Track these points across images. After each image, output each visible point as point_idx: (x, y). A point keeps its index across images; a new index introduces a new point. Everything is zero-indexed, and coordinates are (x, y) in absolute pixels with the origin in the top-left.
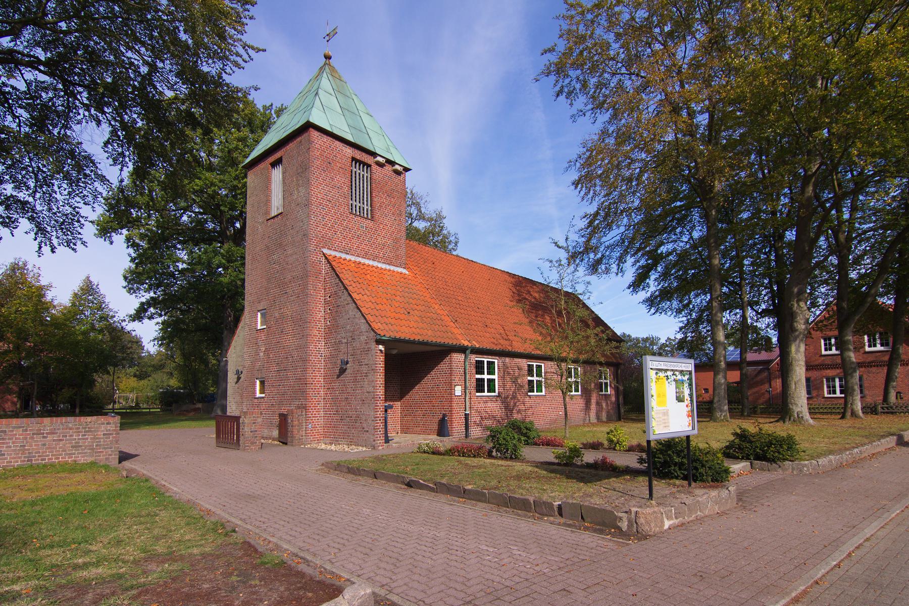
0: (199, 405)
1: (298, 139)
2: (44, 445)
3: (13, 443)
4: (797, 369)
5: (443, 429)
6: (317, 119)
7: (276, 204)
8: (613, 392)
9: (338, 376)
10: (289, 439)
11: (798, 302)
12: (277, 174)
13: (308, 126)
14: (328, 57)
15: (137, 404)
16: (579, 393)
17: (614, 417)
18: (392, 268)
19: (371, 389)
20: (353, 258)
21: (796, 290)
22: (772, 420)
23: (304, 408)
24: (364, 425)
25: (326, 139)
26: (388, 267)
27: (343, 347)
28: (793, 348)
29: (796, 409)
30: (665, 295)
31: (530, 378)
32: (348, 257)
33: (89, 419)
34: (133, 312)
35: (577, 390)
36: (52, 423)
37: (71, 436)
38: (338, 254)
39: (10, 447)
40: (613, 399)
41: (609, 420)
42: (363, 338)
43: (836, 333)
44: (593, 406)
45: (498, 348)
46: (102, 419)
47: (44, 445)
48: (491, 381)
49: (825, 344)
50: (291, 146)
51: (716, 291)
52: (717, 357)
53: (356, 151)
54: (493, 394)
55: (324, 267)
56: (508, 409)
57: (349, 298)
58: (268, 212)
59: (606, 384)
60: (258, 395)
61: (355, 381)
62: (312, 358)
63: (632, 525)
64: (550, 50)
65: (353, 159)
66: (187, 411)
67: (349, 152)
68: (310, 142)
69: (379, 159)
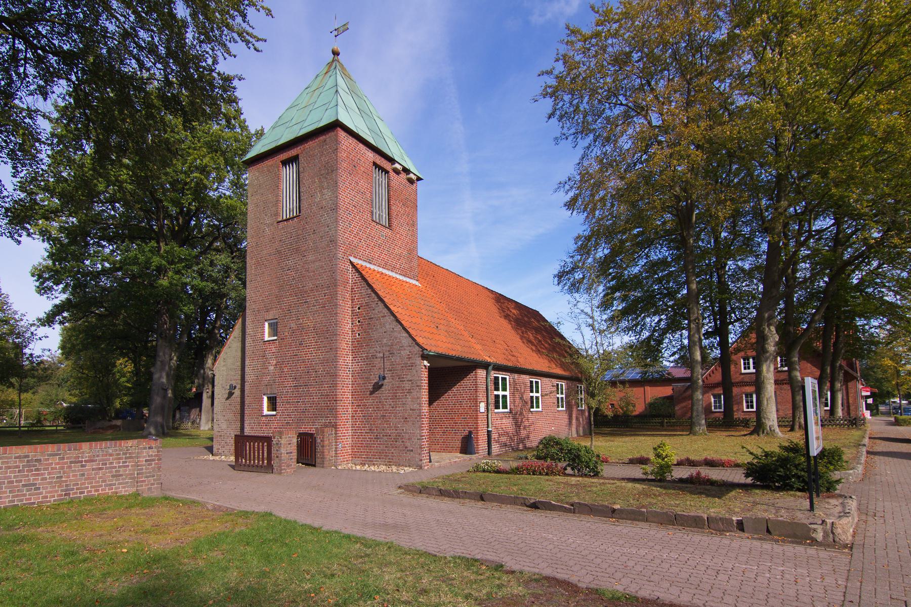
0: (119, 422)
1: (322, 138)
2: (83, 475)
3: (49, 474)
4: (769, 386)
5: (467, 446)
7: (288, 205)
9: (372, 393)
10: (318, 461)
11: (768, 326)
12: (288, 174)
13: (336, 125)
14: (336, 53)
15: (39, 421)
19: (416, 406)
20: (376, 268)
21: (766, 315)
22: (743, 433)
23: (335, 426)
24: (408, 444)
25: (351, 140)
28: (765, 368)
29: (768, 423)
31: (496, 393)
33: (130, 443)
34: (42, 315)
37: (111, 463)
38: (364, 264)
39: (46, 479)
40: (587, 414)
41: (585, 435)
42: (405, 353)
43: (754, 353)
44: (574, 421)
46: (144, 443)
47: (83, 475)
48: (504, 397)
49: (744, 364)
50: (311, 144)
51: (694, 313)
52: (695, 375)
53: (377, 156)
55: (351, 274)
58: (277, 214)
60: (266, 412)
61: (395, 397)
62: (341, 373)
63: (828, 535)
64: (549, 73)
65: (375, 164)
66: (103, 429)
67: (371, 156)
68: (337, 142)
69: (397, 165)
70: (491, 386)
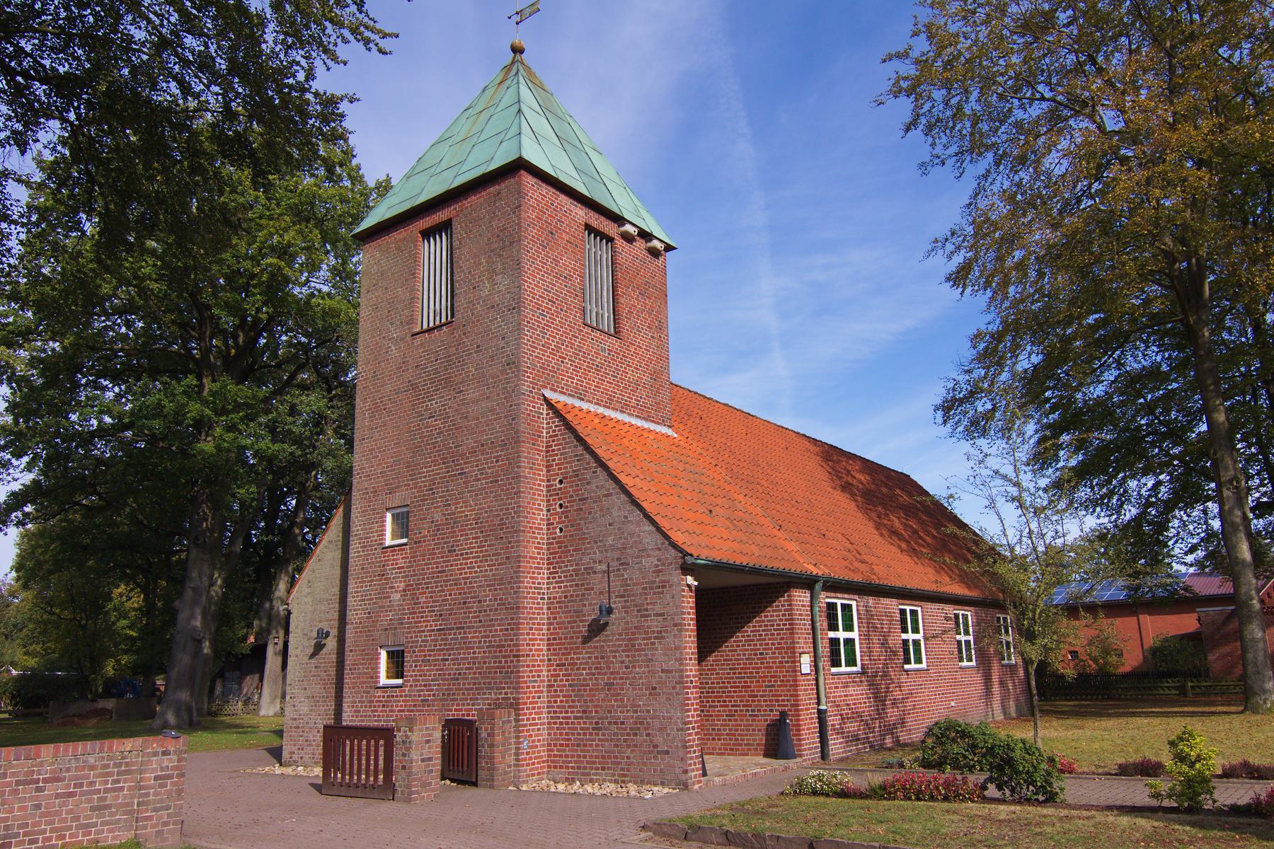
0: (110, 704)
6: (533, 155)
8: (1020, 661)
12: (433, 253)
13: (520, 166)
14: (517, 50)
16: (973, 663)
17: (1025, 710)
18: (652, 426)
19: (673, 664)
20: (592, 408)
23: (515, 706)
24: (659, 740)
25: (546, 190)
26: (646, 425)
27: (598, 582)
30: (1081, 473)
31: (832, 634)
32: (585, 406)
35: (970, 660)
36: (56, 755)
38: (570, 401)
40: (1021, 673)
44: (996, 688)
45: (857, 578)
47: (38, 807)
50: (473, 200)
51: (1227, 469)
52: (1243, 590)
53: (592, 213)
54: (854, 669)
56: (879, 698)
57: (611, 485)
58: (411, 321)
59: (1008, 643)
60: (383, 680)
61: (631, 647)
62: (527, 603)
65: (588, 227)
66: (80, 716)
67: (580, 213)
68: (520, 194)
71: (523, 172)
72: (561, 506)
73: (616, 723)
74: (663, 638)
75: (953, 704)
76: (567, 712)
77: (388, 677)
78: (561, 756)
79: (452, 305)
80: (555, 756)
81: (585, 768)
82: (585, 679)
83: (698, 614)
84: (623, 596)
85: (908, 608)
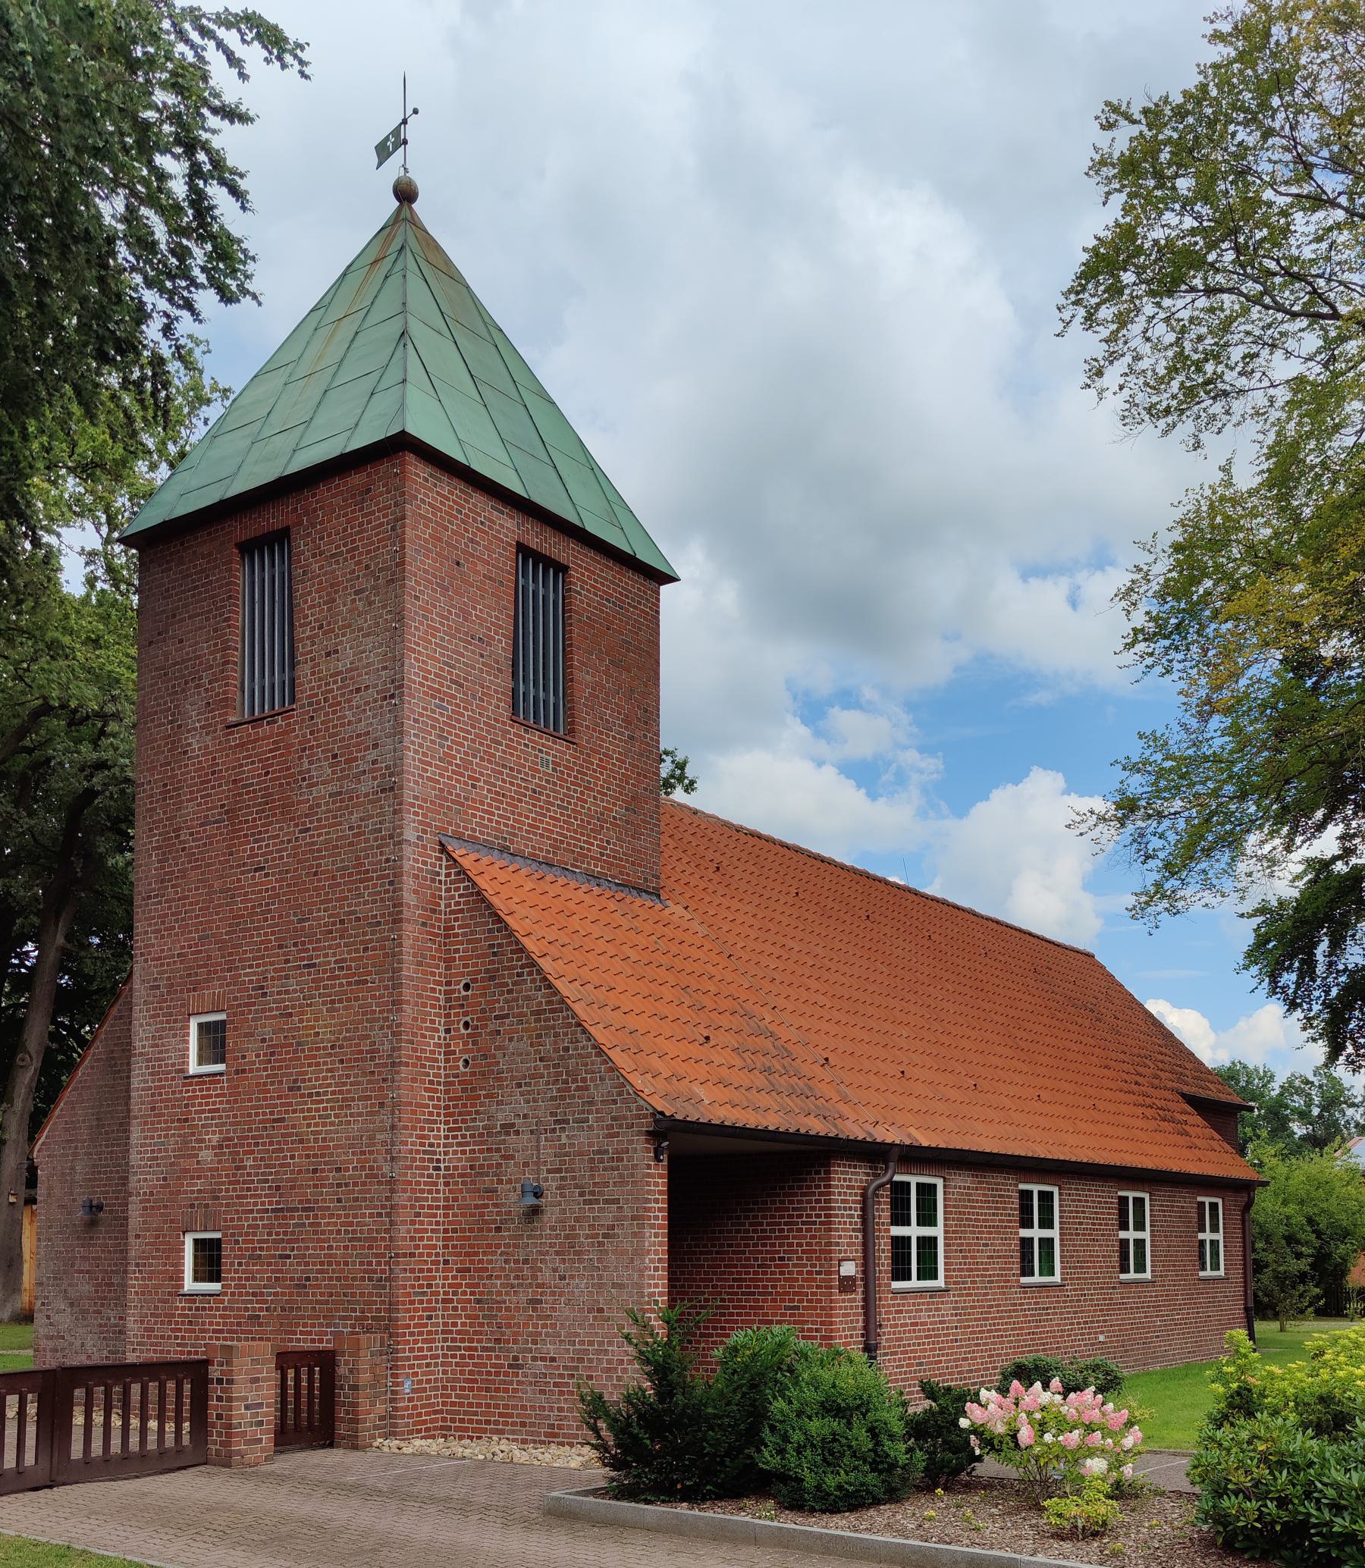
10: (342, 1429)
25: (448, 488)
31: (897, 1231)
65: (522, 549)
70: (883, 1211)
71: (410, 458)
72: (466, 1025)
73: (543, 1359)
74: (614, 1236)
75: (1101, 1338)
76: (471, 1341)
77: (196, 1279)
78: (461, 1405)
79: (292, 681)
80: (453, 1404)
81: (497, 1423)
82: (499, 1293)
83: (670, 1201)
84: (559, 1171)
85: (1036, 1188)
